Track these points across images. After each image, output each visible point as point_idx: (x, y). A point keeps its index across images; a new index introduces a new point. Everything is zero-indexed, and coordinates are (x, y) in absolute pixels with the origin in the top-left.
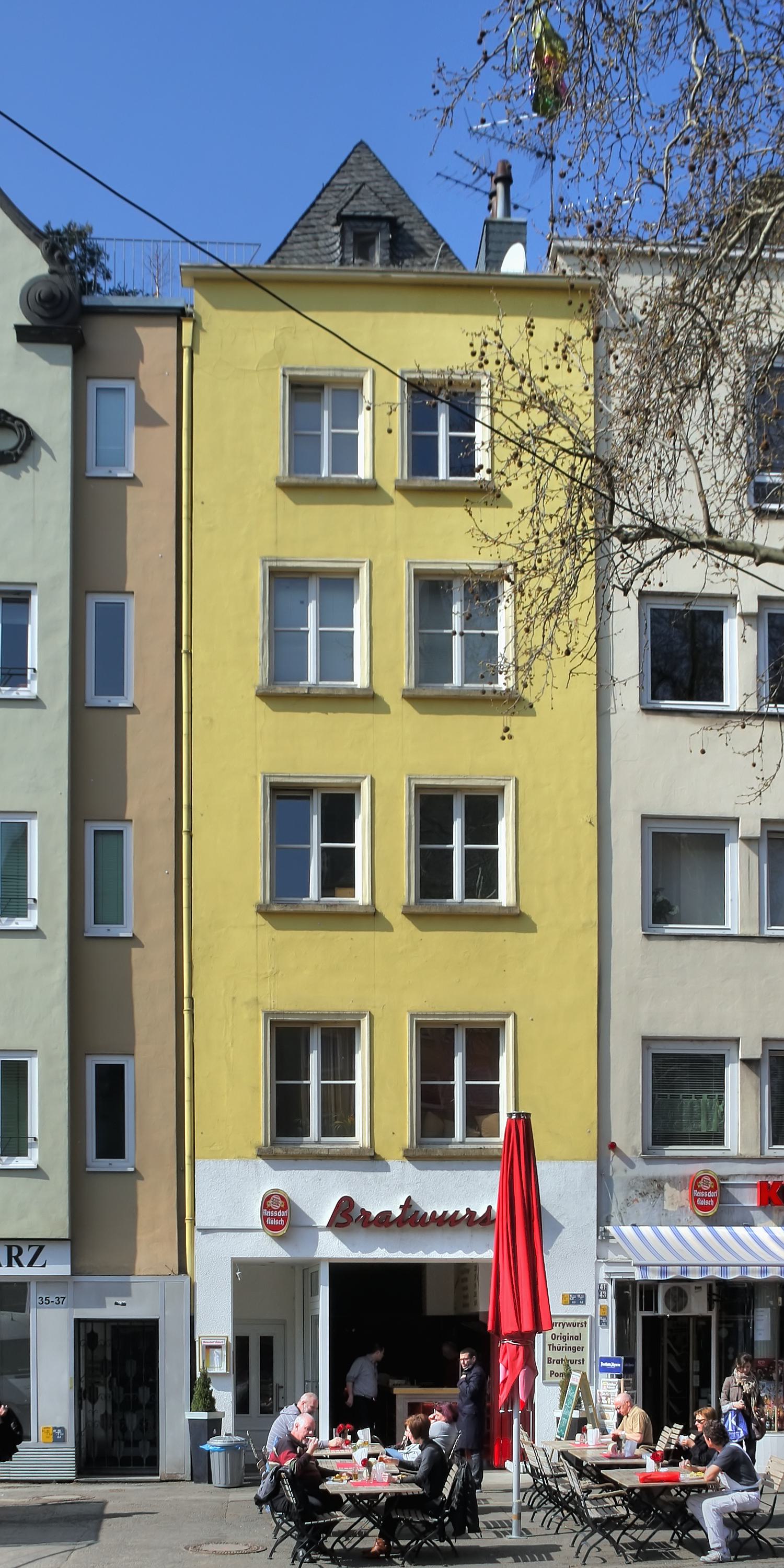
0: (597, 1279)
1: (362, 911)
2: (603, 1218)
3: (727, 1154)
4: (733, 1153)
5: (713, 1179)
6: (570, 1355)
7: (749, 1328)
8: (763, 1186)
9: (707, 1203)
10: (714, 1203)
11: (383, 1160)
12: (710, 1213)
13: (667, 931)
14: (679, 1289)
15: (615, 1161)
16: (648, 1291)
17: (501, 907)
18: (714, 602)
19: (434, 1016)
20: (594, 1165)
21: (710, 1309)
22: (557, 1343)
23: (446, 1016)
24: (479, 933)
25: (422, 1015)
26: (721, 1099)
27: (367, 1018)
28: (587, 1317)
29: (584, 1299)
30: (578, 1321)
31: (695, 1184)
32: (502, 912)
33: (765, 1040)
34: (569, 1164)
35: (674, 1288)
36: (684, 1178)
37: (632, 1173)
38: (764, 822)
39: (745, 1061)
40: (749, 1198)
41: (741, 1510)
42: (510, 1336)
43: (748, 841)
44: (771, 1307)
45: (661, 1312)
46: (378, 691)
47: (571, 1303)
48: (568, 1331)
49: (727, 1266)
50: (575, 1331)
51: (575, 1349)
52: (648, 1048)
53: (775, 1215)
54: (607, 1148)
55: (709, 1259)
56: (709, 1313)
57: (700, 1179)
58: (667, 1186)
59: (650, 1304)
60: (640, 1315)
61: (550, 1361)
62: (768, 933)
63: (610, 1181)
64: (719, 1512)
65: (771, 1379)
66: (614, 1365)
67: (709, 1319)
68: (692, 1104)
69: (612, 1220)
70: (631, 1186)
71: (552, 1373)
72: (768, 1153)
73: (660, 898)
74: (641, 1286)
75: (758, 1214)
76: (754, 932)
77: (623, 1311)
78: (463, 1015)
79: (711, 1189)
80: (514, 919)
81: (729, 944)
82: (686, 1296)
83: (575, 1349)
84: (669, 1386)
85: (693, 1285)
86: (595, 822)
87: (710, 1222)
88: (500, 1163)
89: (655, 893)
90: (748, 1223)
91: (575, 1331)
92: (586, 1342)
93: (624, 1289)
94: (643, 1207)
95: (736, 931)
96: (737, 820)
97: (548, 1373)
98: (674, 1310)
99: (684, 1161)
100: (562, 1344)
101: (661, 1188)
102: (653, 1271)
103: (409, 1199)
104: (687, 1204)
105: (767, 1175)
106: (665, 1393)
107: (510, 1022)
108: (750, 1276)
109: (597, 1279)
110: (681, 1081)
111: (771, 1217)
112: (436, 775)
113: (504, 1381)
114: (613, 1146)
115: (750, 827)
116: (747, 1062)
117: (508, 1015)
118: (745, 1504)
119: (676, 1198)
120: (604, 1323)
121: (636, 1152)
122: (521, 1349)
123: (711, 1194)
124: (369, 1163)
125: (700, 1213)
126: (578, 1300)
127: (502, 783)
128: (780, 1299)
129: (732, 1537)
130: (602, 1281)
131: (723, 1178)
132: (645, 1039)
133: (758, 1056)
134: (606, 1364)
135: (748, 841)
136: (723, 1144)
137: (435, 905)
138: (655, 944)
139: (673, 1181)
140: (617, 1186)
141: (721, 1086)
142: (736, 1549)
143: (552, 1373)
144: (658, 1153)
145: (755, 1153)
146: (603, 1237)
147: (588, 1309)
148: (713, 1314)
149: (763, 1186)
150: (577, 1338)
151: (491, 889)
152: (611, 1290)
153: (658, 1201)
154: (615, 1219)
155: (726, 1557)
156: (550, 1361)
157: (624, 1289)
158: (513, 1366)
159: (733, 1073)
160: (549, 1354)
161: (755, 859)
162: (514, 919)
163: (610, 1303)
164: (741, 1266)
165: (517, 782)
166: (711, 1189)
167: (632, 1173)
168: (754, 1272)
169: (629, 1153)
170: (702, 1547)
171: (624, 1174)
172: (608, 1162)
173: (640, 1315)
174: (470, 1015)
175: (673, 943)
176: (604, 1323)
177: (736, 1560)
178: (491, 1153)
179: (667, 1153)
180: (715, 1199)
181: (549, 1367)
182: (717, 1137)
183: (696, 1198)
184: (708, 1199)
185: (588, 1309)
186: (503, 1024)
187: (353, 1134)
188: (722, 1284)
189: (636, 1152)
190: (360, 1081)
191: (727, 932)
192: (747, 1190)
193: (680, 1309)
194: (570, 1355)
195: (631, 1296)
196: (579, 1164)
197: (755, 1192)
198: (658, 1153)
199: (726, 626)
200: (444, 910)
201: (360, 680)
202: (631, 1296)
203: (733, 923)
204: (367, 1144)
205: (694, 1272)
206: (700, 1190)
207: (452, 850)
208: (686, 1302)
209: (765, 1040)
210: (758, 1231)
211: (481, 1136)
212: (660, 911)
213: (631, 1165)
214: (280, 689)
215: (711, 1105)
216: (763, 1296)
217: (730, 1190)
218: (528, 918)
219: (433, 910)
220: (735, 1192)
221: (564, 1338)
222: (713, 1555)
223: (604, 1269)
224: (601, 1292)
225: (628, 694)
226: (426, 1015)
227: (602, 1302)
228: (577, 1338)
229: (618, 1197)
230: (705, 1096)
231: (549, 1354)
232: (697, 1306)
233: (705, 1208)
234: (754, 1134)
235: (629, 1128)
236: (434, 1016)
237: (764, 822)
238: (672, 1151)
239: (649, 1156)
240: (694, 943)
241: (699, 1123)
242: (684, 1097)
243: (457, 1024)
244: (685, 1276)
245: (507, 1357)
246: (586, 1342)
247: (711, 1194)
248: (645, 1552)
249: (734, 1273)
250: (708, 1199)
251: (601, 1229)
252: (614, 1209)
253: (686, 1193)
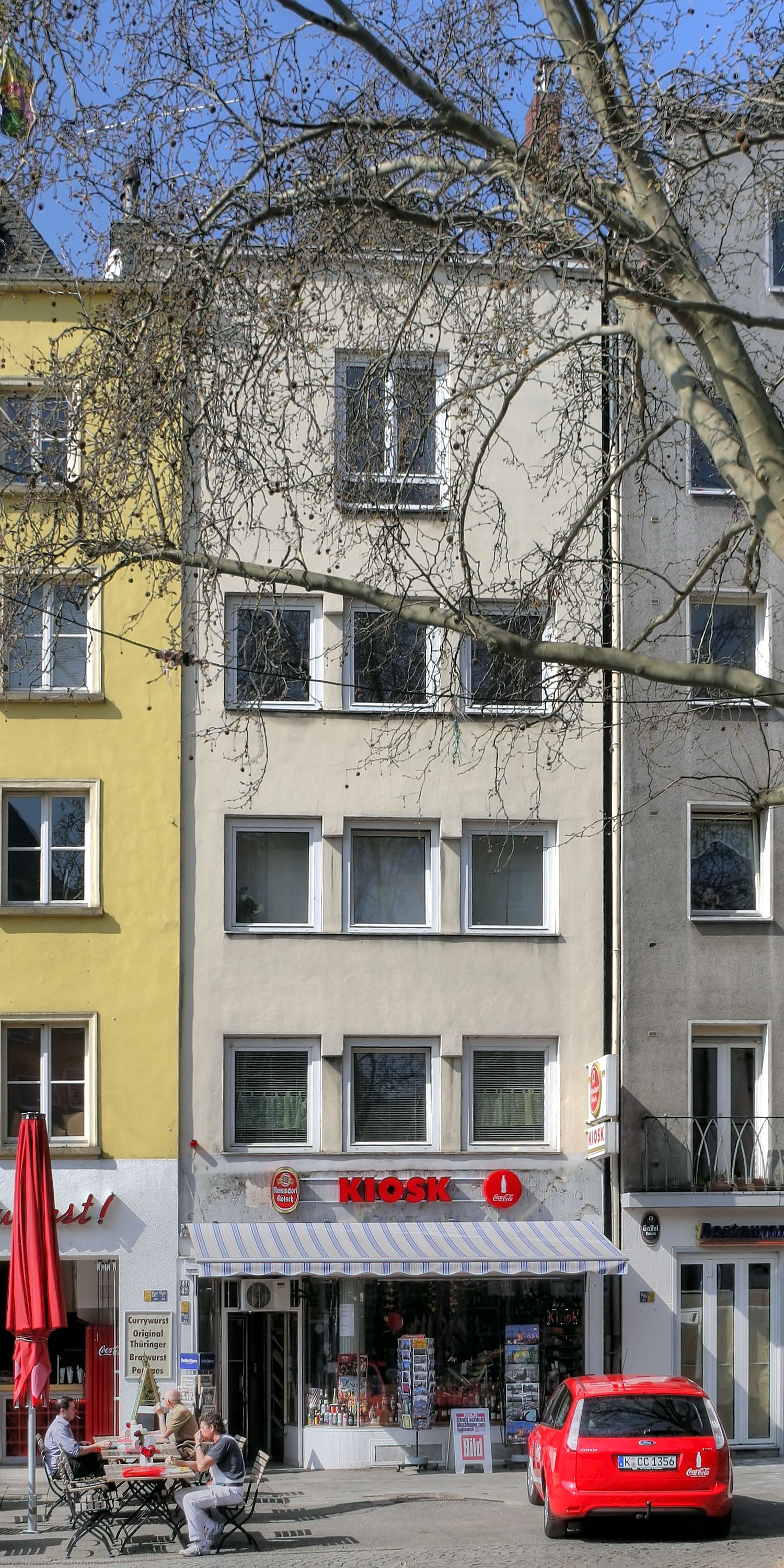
0: (178, 1275)
1: (90, 913)
2: (185, 1216)
3: (309, 1150)
4: (316, 1149)
5: (292, 1176)
6: (150, 1352)
7: (334, 1325)
8: (343, 1183)
9: (287, 1199)
10: (294, 1197)
11: (112, 1158)
12: (290, 1210)
13: (251, 930)
14: (261, 1289)
15: (198, 1159)
16: (233, 1286)
17: (87, 909)
18: (300, 602)
19: (19, 1016)
20: (175, 1163)
21: (295, 1303)
22: (139, 1339)
23: (31, 1016)
24: (64, 935)
25: (8, 1016)
26: (304, 1096)
27: (94, 1019)
28: (168, 1313)
29: (166, 1296)
30: (160, 1317)
31: (276, 1180)
32: (85, 913)
33: (346, 1037)
34: (150, 1163)
35: (257, 1284)
36: (266, 1175)
37: (213, 1170)
38: (347, 820)
39: (327, 1058)
40: (331, 1195)
41: (222, 1504)
42: (24, 1333)
43: (331, 839)
44: (354, 1302)
45: (243, 1309)
46: (110, 697)
47: (153, 1300)
48: (150, 1327)
49: (527, 1261)
50: (156, 1328)
51: (157, 1346)
52: (231, 1047)
53: (356, 1211)
54: (187, 1146)
55: (489, 1254)
56: (294, 1309)
57: (279, 1176)
58: (248, 1183)
59: (234, 1302)
60: (225, 1311)
61: (132, 1357)
62: (351, 930)
63: (192, 1179)
64: (197, 1506)
65: (355, 1375)
66: (192, 1361)
67: (294, 1315)
68: (275, 1101)
69: (194, 1217)
70: (212, 1183)
71: (134, 1369)
72: (351, 1149)
73: (244, 897)
74: (226, 1284)
75: (340, 1211)
76: (337, 929)
77: (207, 1307)
78: (47, 1016)
79: (291, 1186)
80: (99, 920)
81: (311, 942)
82: (269, 1292)
83: (157, 1346)
84: (273, 1380)
85: (276, 1281)
86: (178, 823)
87: (292, 1218)
88: (15, 1163)
89: (239, 893)
90: (329, 1219)
91: (156, 1328)
92: (168, 1338)
93: (203, 1284)
94: (225, 1203)
95: (318, 929)
96: (320, 818)
97: (130, 1369)
98: (256, 1306)
99: (266, 1158)
100: (144, 1340)
101: (242, 1185)
102: (217, 1269)
103: (91, 1197)
104: (269, 1200)
105: (348, 1172)
106: (269, 1390)
107: (93, 1022)
108: (473, 1272)
109: (178, 1275)
110: (263, 1076)
111: (352, 1214)
112: (23, 778)
113: (19, 1377)
114: (194, 1144)
115: (333, 825)
116: (331, 1060)
117: (91, 1015)
118: (225, 1498)
119: (257, 1194)
120: (186, 1319)
121: (217, 1150)
122: (34, 1345)
123: (291, 1191)
124: (97, 1162)
125: (281, 1210)
126: (160, 1296)
127: (87, 785)
128: (362, 1295)
129: (217, 1531)
130: (184, 1277)
131: (304, 1176)
132: (226, 1037)
133: (340, 1053)
134: (186, 1361)
135: (331, 839)
136: (305, 1141)
137: (22, 907)
138: (236, 942)
139: (255, 1178)
140: (199, 1183)
141: (303, 1083)
142: (220, 1544)
143: (134, 1369)
144: (241, 1150)
145: (337, 1149)
146: (183, 1234)
147: (169, 1306)
148: (299, 1310)
149: (343, 1183)
150: (159, 1335)
151: (77, 892)
152: (192, 1287)
153: (240, 1198)
154: (197, 1216)
155: (205, 1550)
156: (132, 1357)
157: (203, 1284)
158: (26, 1363)
159: (316, 1071)
160: (131, 1350)
161: (338, 857)
162: (99, 920)
163: (192, 1299)
164: (423, 1262)
165: (101, 783)
166: (291, 1186)
167: (213, 1170)
168: (317, 1269)
169: (210, 1151)
170: (185, 1541)
171: (205, 1172)
172: (190, 1159)
173: (225, 1311)
174: (54, 1015)
175: (255, 942)
176: (186, 1319)
177: (218, 1553)
178: (73, 1152)
179: (250, 1151)
180: (294, 1196)
181: (132, 1364)
182: (300, 1135)
183: (276, 1195)
184: (288, 1195)
185: (169, 1306)
186: (87, 1023)
187: (82, 1133)
188: (308, 1279)
189: (217, 1150)
190: (89, 1082)
191: (310, 930)
192: (328, 1187)
193: (262, 1306)
194: (150, 1352)
195: (212, 1293)
196: (160, 1162)
197: (337, 1188)
198: (241, 1150)
199: (313, 627)
200: (29, 911)
201: (92, 685)
202: (212, 1293)
203: (316, 921)
204: (94, 1142)
205: (257, 1269)
206: (280, 1187)
207: (39, 852)
208: (269, 1299)
209: (346, 1037)
210: (338, 1228)
211: (66, 1135)
212: (244, 910)
213: (213, 1163)
214: (13, 696)
215: (294, 1102)
216: (347, 1292)
217: (311, 1186)
218: (112, 919)
219: (19, 912)
220: (316, 1189)
221: (147, 1335)
222: (193, 1548)
223: (185, 1265)
224: (182, 1288)
225: (212, 697)
226: (12, 1016)
227: (184, 1299)
228: (159, 1335)
229: (201, 1192)
230: (288, 1093)
231: (131, 1350)
232: (280, 1302)
233: (282, 1205)
234: (336, 1131)
235: (210, 1126)
236: (19, 1016)
237: (347, 820)
238: (255, 1148)
239: (230, 1153)
240: (276, 941)
241: (282, 1120)
242: (268, 1094)
243: (43, 1024)
244: (248, 1273)
245: (21, 1354)
246: (168, 1338)
247: (291, 1191)
248: (145, 1546)
249: (297, 1269)
250: (288, 1195)
251: (183, 1226)
252: (196, 1207)
253: (267, 1190)
